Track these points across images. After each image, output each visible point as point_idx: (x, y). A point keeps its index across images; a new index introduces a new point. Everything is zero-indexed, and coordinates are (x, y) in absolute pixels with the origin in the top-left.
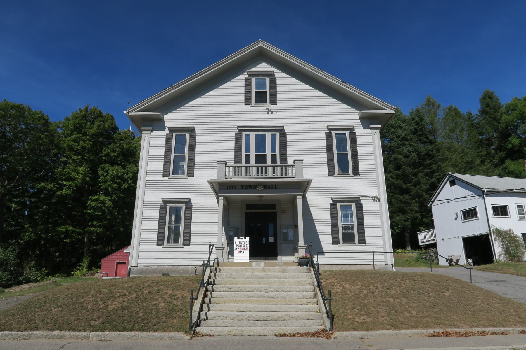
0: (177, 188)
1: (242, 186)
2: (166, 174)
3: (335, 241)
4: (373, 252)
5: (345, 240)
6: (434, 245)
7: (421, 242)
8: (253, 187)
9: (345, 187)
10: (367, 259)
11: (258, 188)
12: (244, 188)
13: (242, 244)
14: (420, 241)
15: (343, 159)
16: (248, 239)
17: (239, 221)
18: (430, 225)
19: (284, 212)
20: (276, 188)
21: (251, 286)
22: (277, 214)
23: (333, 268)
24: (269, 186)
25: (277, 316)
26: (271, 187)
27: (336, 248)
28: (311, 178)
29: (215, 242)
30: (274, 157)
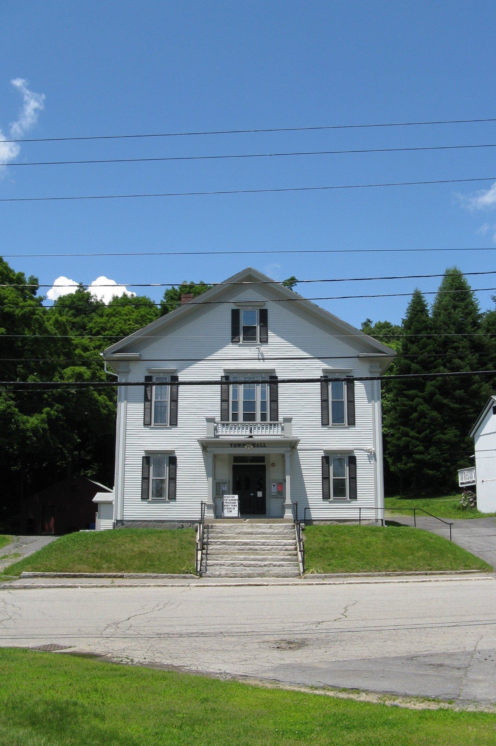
0: (160, 440)
1: (231, 444)
2: (147, 424)
3: (326, 496)
4: (360, 508)
5: (335, 495)
6: (473, 489)
7: (462, 483)
8: (242, 446)
9: (339, 439)
10: (353, 514)
11: (246, 447)
12: (233, 446)
13: (232, 503)
14: (460, 482)
15: (338, 405)
16: (236, 497)
17: (226, 474)
18: (472, 463)
19: (273, 465)
20: (264, 447)
21: (242, 541)
22: (267, 467)
23: (107, 582)
24: (258, 445)
25: (263, 565)
26: (260, 445)
27: (326, 504)
28: (299, 438)
29: (204, 501)
30: (263, 404)
